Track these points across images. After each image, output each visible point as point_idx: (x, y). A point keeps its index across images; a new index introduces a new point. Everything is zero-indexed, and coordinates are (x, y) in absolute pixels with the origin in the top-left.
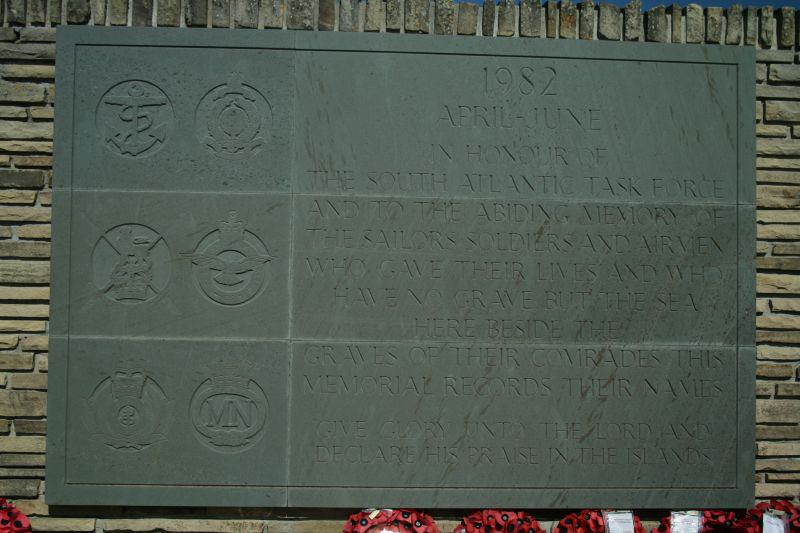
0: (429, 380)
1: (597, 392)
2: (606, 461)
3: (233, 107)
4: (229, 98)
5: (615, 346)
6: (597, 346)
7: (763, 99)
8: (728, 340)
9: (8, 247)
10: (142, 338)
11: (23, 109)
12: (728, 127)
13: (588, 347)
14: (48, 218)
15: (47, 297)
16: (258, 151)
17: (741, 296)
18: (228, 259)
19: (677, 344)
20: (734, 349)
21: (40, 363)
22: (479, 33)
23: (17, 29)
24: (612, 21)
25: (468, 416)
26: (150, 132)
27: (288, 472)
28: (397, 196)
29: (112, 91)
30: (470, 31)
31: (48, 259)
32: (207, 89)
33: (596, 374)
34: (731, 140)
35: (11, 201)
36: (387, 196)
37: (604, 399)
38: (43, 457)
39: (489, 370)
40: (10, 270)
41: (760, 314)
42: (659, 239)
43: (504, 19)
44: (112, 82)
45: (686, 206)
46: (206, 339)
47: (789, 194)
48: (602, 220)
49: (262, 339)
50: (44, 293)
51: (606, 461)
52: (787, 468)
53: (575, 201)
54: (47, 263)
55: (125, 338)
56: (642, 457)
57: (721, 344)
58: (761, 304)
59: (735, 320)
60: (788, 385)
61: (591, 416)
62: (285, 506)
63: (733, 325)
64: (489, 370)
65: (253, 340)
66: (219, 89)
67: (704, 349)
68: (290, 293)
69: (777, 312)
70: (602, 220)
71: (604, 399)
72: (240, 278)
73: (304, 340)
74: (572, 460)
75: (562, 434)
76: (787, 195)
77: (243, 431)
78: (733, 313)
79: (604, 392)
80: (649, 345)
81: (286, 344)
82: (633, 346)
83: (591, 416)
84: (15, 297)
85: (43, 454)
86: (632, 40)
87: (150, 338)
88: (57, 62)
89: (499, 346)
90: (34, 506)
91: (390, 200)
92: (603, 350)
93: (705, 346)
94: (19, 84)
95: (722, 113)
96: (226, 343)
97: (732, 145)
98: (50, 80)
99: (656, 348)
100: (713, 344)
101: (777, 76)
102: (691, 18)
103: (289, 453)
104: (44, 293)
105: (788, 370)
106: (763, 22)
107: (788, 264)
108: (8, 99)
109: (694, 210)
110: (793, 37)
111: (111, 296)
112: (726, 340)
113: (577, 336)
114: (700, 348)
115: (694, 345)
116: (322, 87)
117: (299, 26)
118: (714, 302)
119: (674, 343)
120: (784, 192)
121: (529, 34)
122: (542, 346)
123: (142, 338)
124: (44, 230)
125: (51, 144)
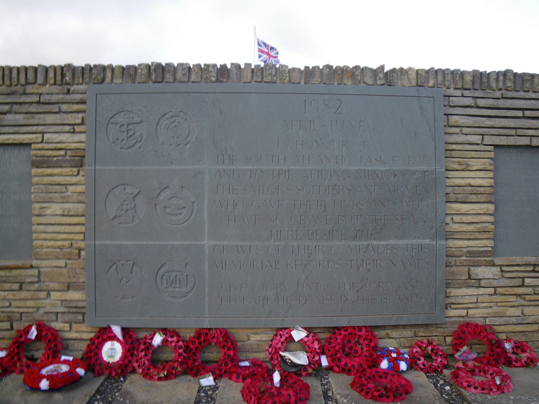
0: (278, 262)
1: (365, 267)
2: (370, 301)
3: (175, 123)
4: (173, 119)
5: (375, 243)
6: (365, 243)
7: (447, 115)
8: (431, 238)
9: (65, 197)
10: (131, 243)
11: (72, 127)
12: (430, 129)
13: (360, 243)
14: (83, 182)
15: (84, 222)
16: (188, 146)
17: (437, 216)
18: (175, 201)
19: (406, 241)
20: (435, 243)
21: (526, 88)
22: (303, 83)
23: (69, 87)
24: (370, 75)
25: (299, 281)
26: (134, 137)
27: (207, 309)
28: (260, 167)
29: (115, 117)
30: (297, 81)
31: (84, 203)
32: (162, 114)
33: (365, 258)
34: (432, 136)
35: (67, 174)
36: (255, 167)
37: (369, 270)
38: (85, 303)
39: (309, 257)
40: (66, 209)
41: (447, 224)
42: (396, 187)
43: (256, 332)
44: (114, 112)
45: (410, 170)
46: (164, 243)
47: (461, 163)
48: (367, 178)
49: (193, 243)
50: (82, 220)
51: (370, 301)
52: (460, 302)
53: (353, 168)
54: (84, 205)
55: (123, 243)
56: (388, 299)
57: (428, 240)
58: (448, 219)
59: (435, 228)
60: (461, 260)
61: (362, 279)
62: (206, 327)
63: (434, 230)
64: (309, 257)
65: (187, 243)
66: (168, 114)
67: (420, 243)
68: (206, 219)
69: (456, 223)
70: (367, 178)
71: (369, 270)
72: (180, 211)
73: (213, 243)
74: (353, 302)
75: (347, 288)
76: (460, 164)
77: (184, 290)
78: (434, 224)
79: (368, 267)
80: (392, 242)
81: (204, 245)
82: (384, 243)
83: (362, 279)
84: (508, 130)
85: (85, 301)
86: (381, 85)
87: (135, 243)
88: (87, 103)
89: (315, 244)
90: (81, 327)
91: (257, 169)
92: (368, 245)
93: (420, 241)
94: (70, 115)
95: (427, 122)
96: (173, 245)
97: (433, 139)
98: (84, 112)
99: (395, 243)
100: (424, 241)
101: (453, 103)
102: (410, 74)
103: (207, 301)
104: (82, 220)
105: (461, 253)
106: (446, 76)
107: (461, 199)
108: (64, 122)
109: (414, 172)
110: (461, 84)
111: (117, 221)
112: (431, 238)
113: (355, 238)
114: (418, 243)
115: (415, 242)
116: (221, 112)
117: (209, 81)
118: (425, 219)
119: (404, 241)
120: (459, 162)
121: (328, 83)
122: (337, 243)
123: (131, 243)
124: (80, 188)
125: (84, 144)
